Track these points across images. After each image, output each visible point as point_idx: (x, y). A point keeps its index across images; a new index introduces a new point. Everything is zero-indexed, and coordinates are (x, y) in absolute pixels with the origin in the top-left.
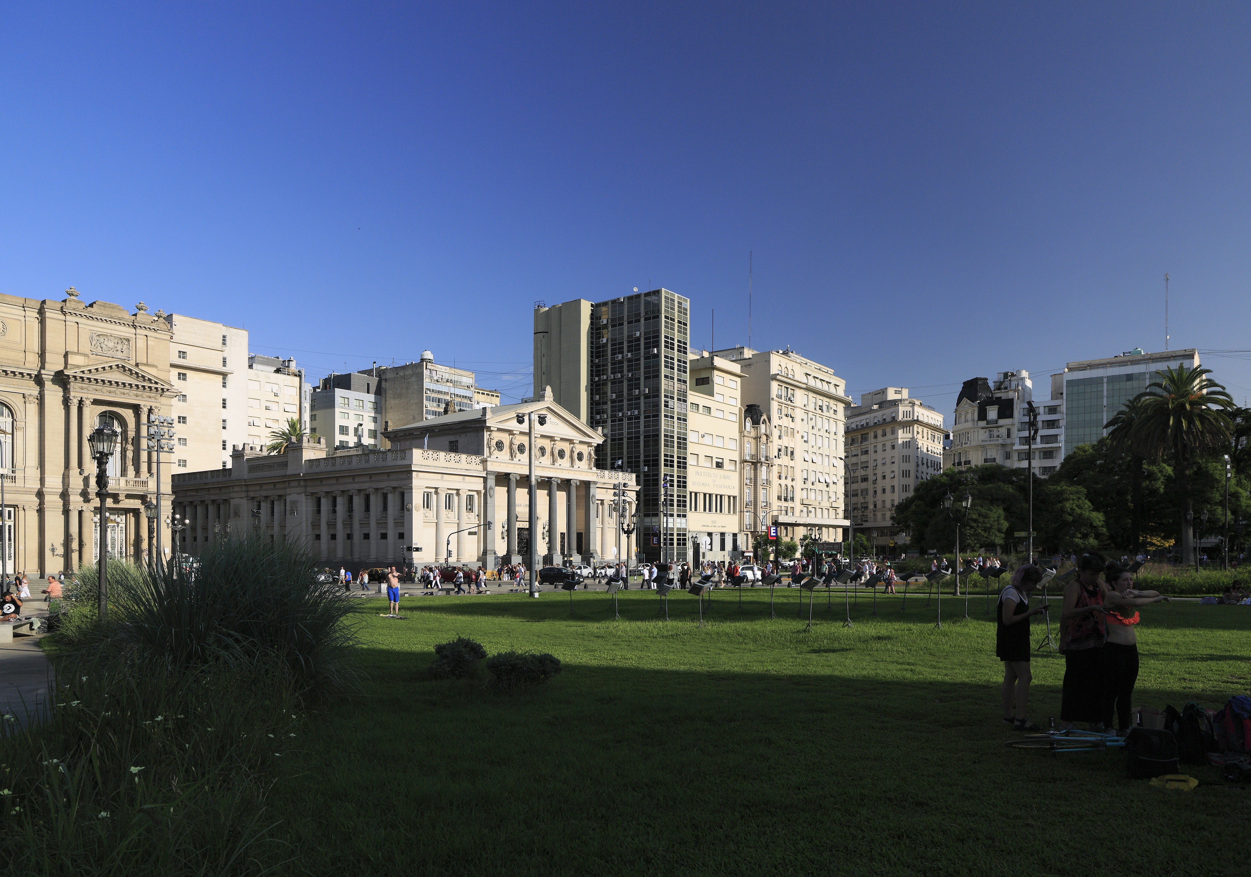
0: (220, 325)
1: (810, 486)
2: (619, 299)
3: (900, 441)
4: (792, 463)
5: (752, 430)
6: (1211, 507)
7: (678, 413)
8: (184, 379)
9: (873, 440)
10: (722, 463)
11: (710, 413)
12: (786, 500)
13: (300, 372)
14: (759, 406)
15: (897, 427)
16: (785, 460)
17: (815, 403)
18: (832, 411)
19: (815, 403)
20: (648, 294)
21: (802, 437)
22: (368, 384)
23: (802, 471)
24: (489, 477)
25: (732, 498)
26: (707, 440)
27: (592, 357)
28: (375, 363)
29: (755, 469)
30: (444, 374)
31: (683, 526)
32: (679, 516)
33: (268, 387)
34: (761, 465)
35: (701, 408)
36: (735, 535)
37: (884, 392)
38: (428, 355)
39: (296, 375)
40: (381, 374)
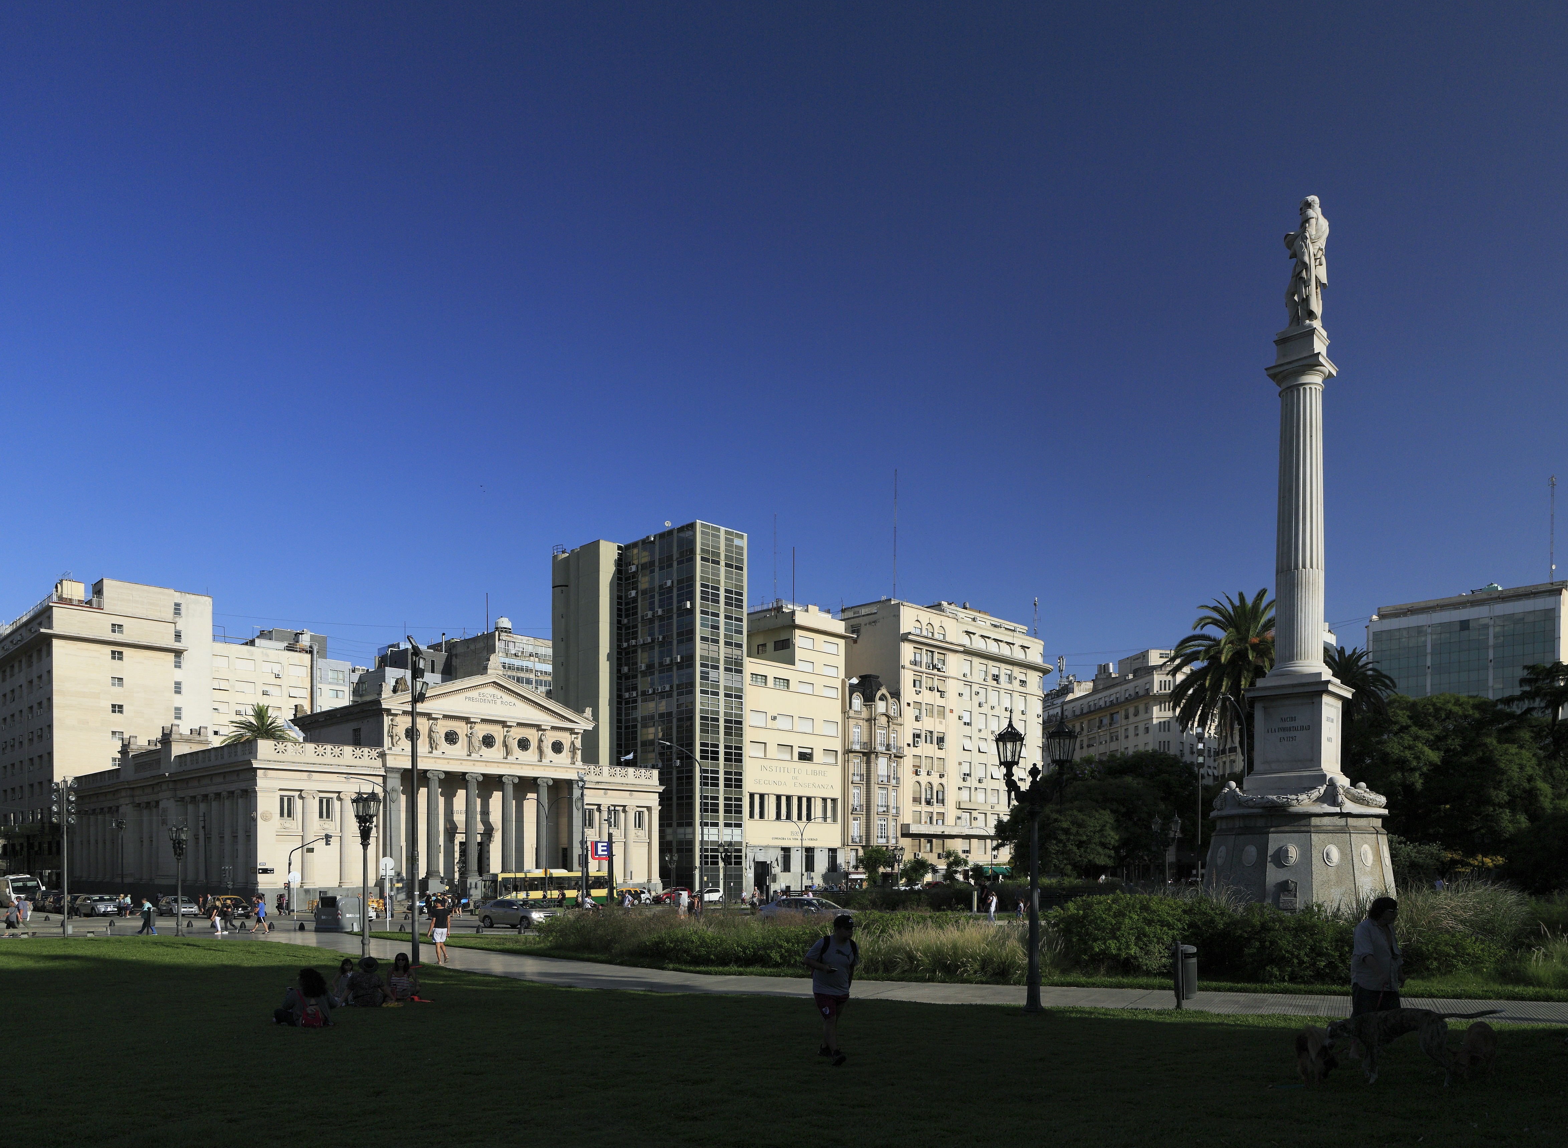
0: (172, 591)
1: (975, 784)
2: (648, 537)
3: (1155, 721)
4: (941, 754)
5: (864, 709)
6: (1495, 810)
7: (726, 688)
8: (121, 659)
9: (1124, 722)
10: (811, 755)
11: (788, 687)
12: (928, 803)
13: (311, 647)
14: (878, 677)
15: (1151, 703)
16: (927, 749)
17: (986, 672)
18: (1016, 683)
19: (986, 672)
20: (681, 529)
21: (960, 718)
22: (433, 662)
23: (960, 764)
24: (389, 775)
25: (829, 801)
26: (781, 723)
27: (619, 615)
28: (444, 634)
29: (868, 762)
30: (525, 646)
31: (737, 839)
32: (727, 825)
33: (267, 667)
34: (877, 757)
35: (770, 681)
36: (833, 851)
37: (1144, 655)
38: (505, 623)
39: (307, 652)
40: (451, 647)
